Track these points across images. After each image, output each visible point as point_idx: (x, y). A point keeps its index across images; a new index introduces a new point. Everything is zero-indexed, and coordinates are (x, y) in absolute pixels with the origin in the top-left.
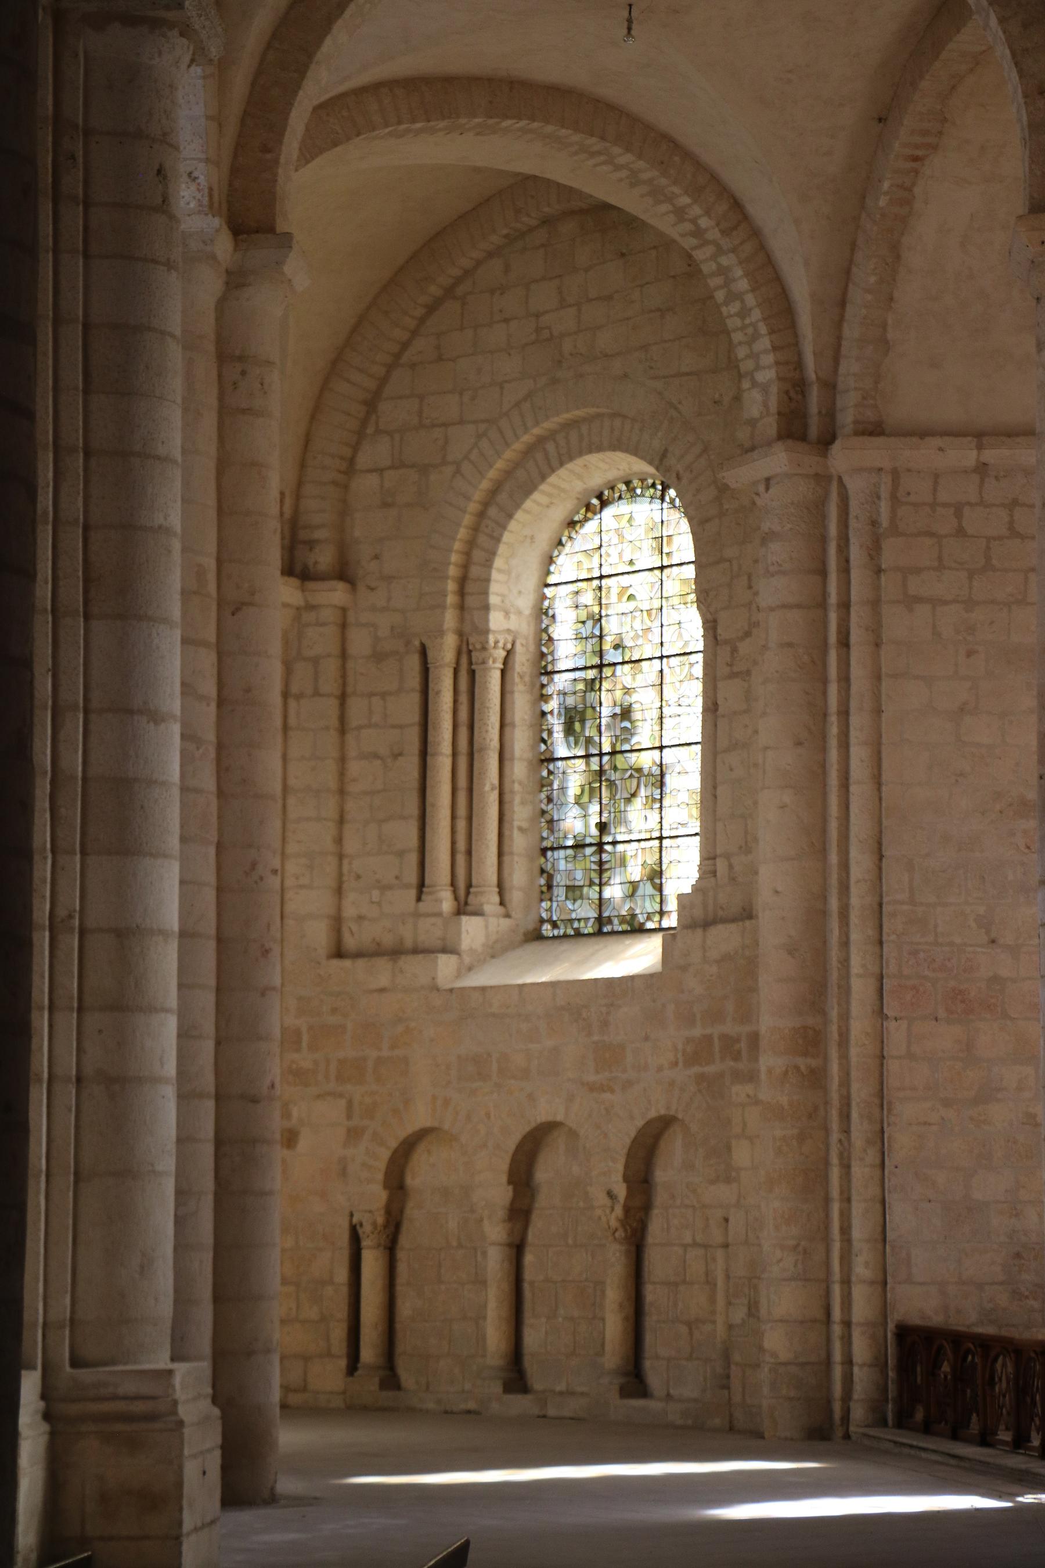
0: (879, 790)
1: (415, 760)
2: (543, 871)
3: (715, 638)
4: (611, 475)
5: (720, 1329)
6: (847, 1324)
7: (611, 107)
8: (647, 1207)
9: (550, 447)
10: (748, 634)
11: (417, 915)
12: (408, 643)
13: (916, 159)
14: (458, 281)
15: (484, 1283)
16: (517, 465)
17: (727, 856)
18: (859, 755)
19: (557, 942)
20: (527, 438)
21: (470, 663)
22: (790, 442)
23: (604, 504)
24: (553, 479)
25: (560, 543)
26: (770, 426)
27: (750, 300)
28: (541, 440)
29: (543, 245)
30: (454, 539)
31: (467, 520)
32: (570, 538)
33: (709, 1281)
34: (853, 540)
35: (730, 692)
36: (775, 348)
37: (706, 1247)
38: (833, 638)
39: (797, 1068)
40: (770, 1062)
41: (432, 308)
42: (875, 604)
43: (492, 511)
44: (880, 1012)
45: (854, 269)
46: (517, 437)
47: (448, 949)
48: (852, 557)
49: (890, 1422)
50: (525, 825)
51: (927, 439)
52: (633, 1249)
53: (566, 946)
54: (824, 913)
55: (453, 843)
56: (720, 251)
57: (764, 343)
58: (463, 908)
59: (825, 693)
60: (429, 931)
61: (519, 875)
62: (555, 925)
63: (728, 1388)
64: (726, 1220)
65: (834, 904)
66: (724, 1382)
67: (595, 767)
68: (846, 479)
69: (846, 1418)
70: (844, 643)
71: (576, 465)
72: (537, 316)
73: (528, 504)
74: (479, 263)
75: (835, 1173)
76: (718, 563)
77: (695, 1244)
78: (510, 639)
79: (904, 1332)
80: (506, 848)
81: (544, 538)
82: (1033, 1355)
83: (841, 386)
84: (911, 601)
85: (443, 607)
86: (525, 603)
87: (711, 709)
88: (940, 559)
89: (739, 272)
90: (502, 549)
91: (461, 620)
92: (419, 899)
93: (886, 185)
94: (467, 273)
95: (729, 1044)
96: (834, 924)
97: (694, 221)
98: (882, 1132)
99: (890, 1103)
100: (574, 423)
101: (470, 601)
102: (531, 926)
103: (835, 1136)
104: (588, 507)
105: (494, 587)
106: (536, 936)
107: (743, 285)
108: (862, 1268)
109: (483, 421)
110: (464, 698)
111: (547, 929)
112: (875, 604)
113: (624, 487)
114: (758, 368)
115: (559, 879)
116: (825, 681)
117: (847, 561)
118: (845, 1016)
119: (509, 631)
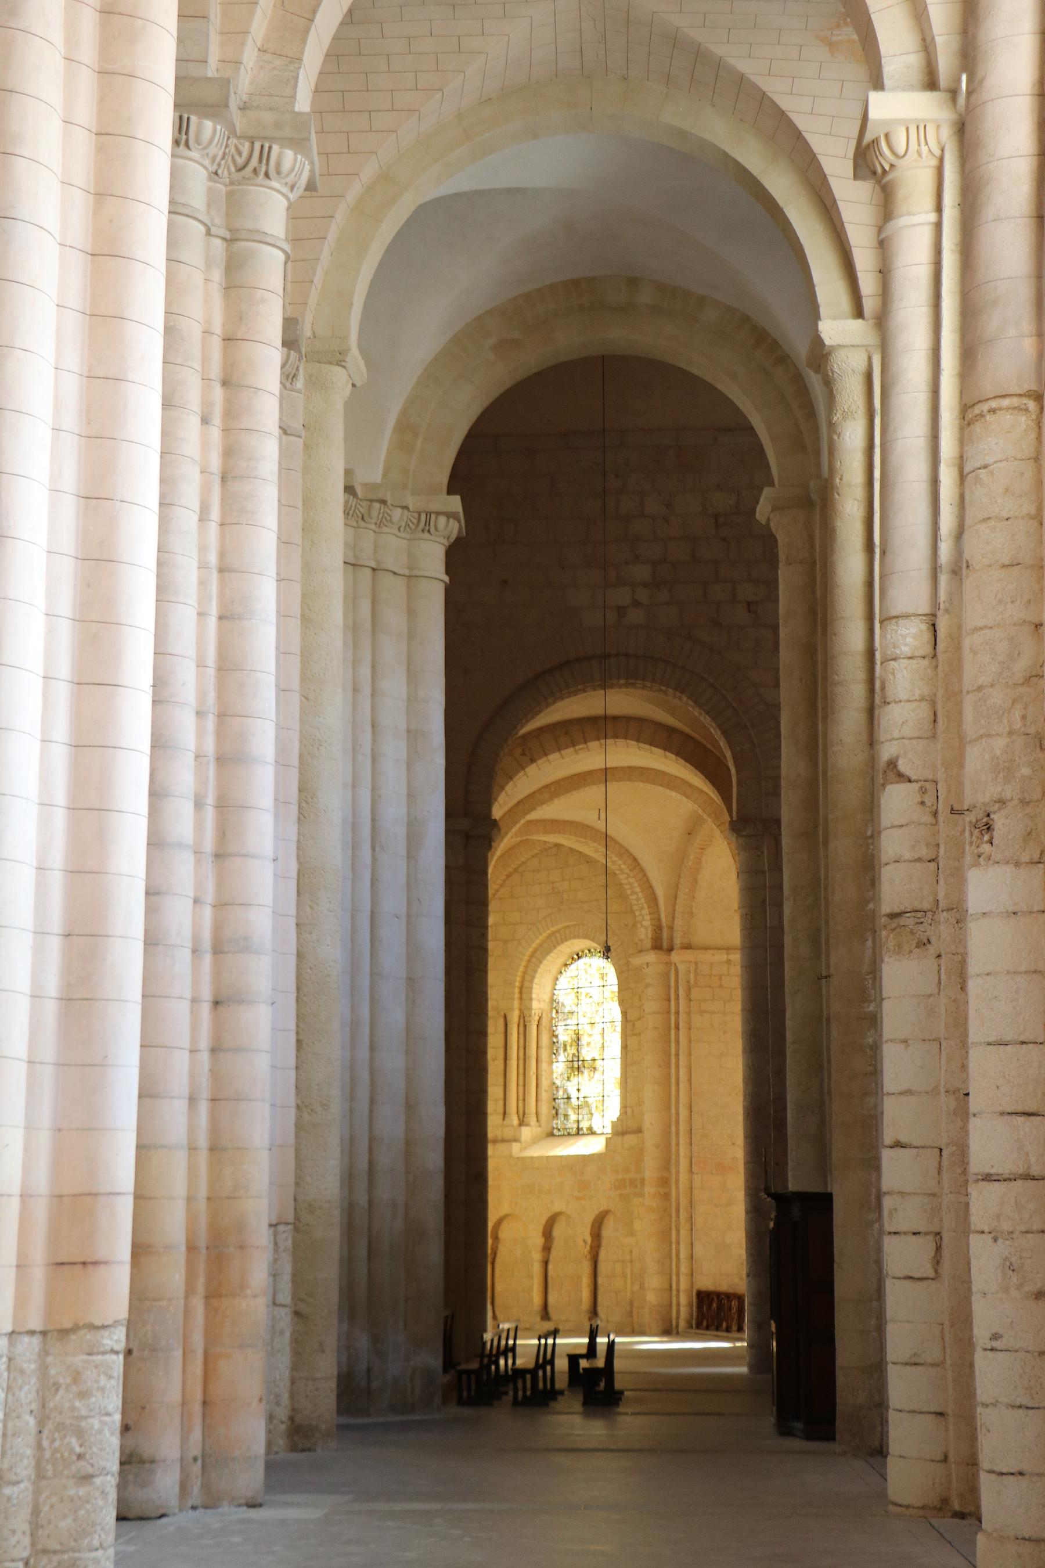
0: (691, 1085)
1: (502, 1061)
2: (554, 1108)
3: (626, 1018)
4: (583, 946)
5: (629, 1294)
6: (678, 1291)
7: (588, 826)
8: (599, 1246)
9: (558, 935)
10: (639, 1019)
11: (503, 1126)
12: (498, 1014)
13: (702, 849)
14: (519, 866)
15: (532, 1277)
16: (544, 941)
17: (631, 1107)
18: (683, 1071)
19: (560, 1138)
20: (548, 932)
21: (524, 1022)
22: (656, 951)
23: (579, 958)
24: (559, 948)
25: (561, 972)
26: (648, 943)
27: (641, 895)
28: (554, 933)
29: (556, 855)
30: (518, 971)
31: (524, 963)
32: (565, 971)
33: (624, 1276)
34: (680, 988)
35: (632, 1041)
36: (650, 914)
37: (623, 1262)
38: (673, 1025)
39: (659, 1192)
40: (649, 1190)
41: (508, 876)
42: (689, 1013)
43: (534, 960)
44: (691, 1171)
45: (680, 886)
46: (545, 932)
47: (516, 1140)
48: (680, 995)
49: (694, 1326)
50: (547, 1089)
51: (708, 951)
52: (593, 1263)
53: (564, 1139)
54: (670, 1132)
55: (518, 1096)
56: (629, 876)
57: (646, 911)
58: (522, 1123)
59: (670, 1047)
60: (508, 1133)
61: (545, 1109)
62: (559, 1130)
63: (632, 1317)
64: (631, 1251)
65: (673, 1129)
66: (630, 1314)
67: (576, 1066)
68: (678, 965)
69: (677, 1326)
70: (677, 1028)
71: (569, 943)
72: (553, 883)
73: (548, 958)
74: (528, 860)
75: (674, 1233)
76: (626, 989)
77: (618, 1261)
78: (540, 1012)
79: (699, 1293)
80: (539, 1098)
81: (554, 970)
82: (723, 1297)
83: (675, 929)
84: (702, 1012)
85: (513, 999)
86: (546, 997)
87: (625, 1047)
88: (713, 996)
89: (636, 885)
90: (537, 975)
91: (521, 1004)
92: (504, 1119)
93: (691, 857)
94: (523, 863)
95: (632, 1182)
96: (674, 1137)
97: (619, 866)
98: (692, 1217)
99: (695, 1206)
100: (568, 926)
101: (524, 996)
102: (549, 1130)
103: (674, 1219)
104: (573, 958)
105: (534, 991)
106: (551, 1135)
107: (638, 889)
108: (684, 1269)
109: (531, 924)
110: (522, 1036)
111: (555, 1132)
112: (689, 1013)
113: (588, 952)
114: (643, 920)
115: (561, 1111)
116: (670, 1042)
117: (678, 995)
118: (678, 1173)
119: (540, 1009)
